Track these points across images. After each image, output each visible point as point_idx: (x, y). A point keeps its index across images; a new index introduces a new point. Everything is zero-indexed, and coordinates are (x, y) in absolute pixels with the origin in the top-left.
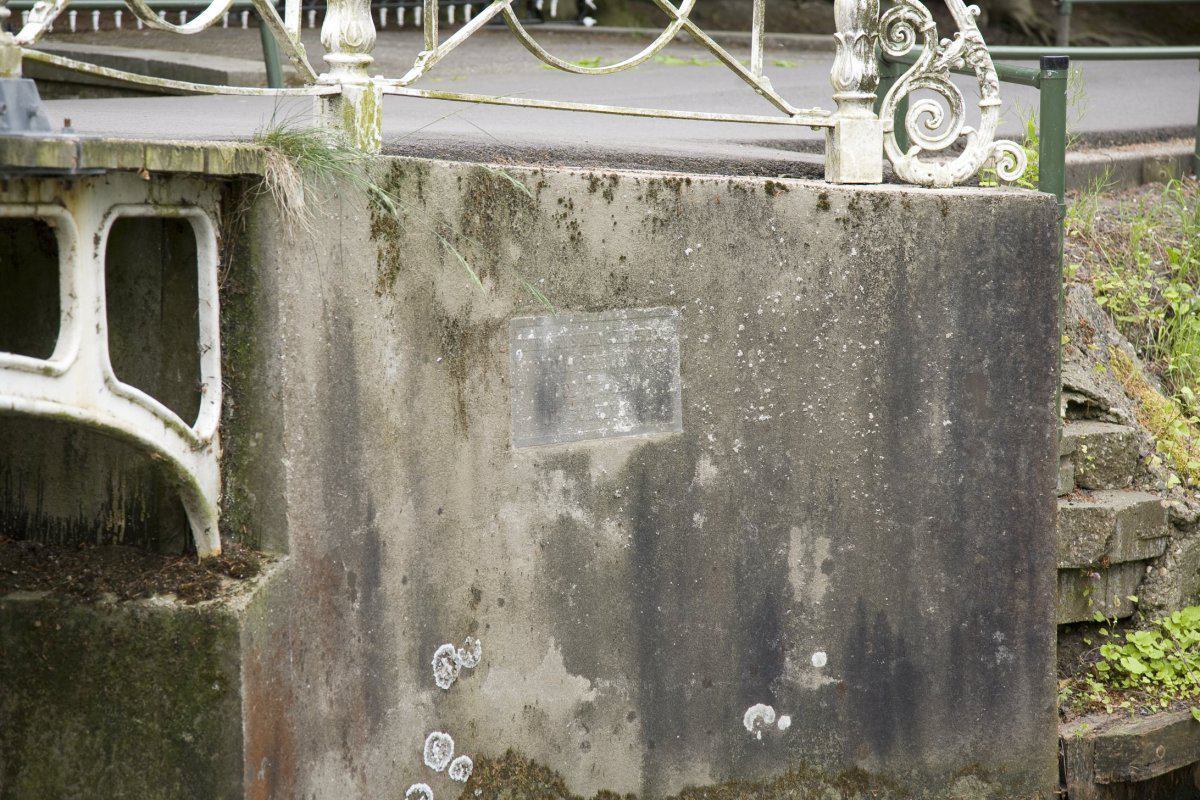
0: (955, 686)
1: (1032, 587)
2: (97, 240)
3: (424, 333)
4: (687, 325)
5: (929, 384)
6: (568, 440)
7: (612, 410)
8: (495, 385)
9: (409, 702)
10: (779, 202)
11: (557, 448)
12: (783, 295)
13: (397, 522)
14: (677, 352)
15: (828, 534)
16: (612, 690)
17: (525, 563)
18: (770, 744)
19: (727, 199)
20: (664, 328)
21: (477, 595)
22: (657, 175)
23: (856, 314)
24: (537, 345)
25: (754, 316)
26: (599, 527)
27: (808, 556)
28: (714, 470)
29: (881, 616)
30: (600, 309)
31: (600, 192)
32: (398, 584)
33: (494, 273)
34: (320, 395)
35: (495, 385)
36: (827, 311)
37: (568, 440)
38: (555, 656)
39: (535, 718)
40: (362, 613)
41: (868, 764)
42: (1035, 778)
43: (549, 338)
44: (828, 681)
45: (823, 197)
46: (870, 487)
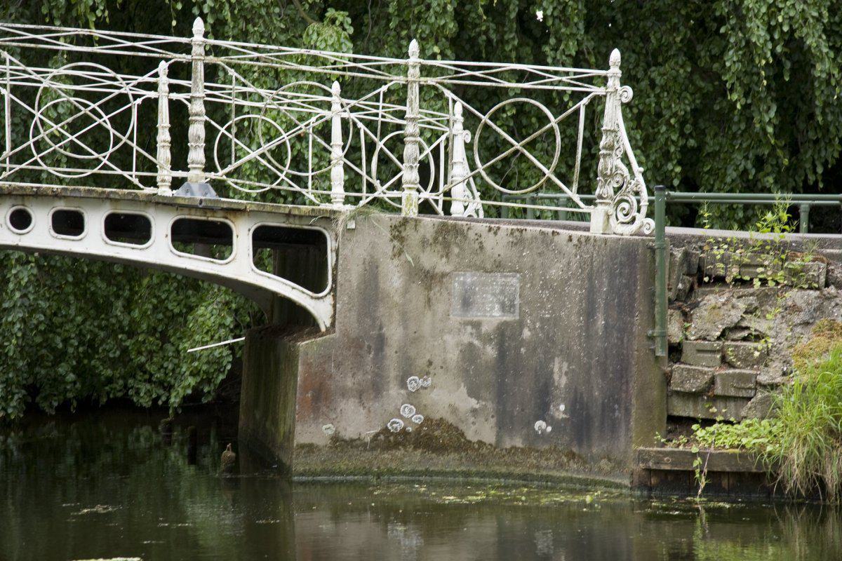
0: (602, 423)
1: (627, 388)
2: (249, 230)
3: (413, 274)
4: (523, 280)
5: (598, 308)
6: (474, 315)
7: (492, 308)
8: (445, 294)
9: (394, 391)
10: (556, 238)
11: (469, 318)
12: (555, 272)
13: (394, 333)
14: (518, 289)
15: (567, 361)
16: (485, 406)
17: (453, 356)
18: (544, 436)
19: (538, 236)
20: (514, 281)
21: (430, 363)
22: (515, 227)
23: (578, 280)
24: (464, 283)
25: (545, 278)
26: (484, 348)
27: (560, 369)
28: (529, 333)
29: (581, 394)
30: (490, 272)
31: (492, 232)
32: (393, 353)
33: (447, 256)
34: (358, 287)
35: (445, 294)
36: (569, 278)
37: (474, 315)
38: (463, 390)
39: (454, 410)
40: (373, 359)
41: (575, 450)
42: (625, 463)
43: (469, 280)
44: (564, 416)
45: (570, 237)
46: (580, 345)
